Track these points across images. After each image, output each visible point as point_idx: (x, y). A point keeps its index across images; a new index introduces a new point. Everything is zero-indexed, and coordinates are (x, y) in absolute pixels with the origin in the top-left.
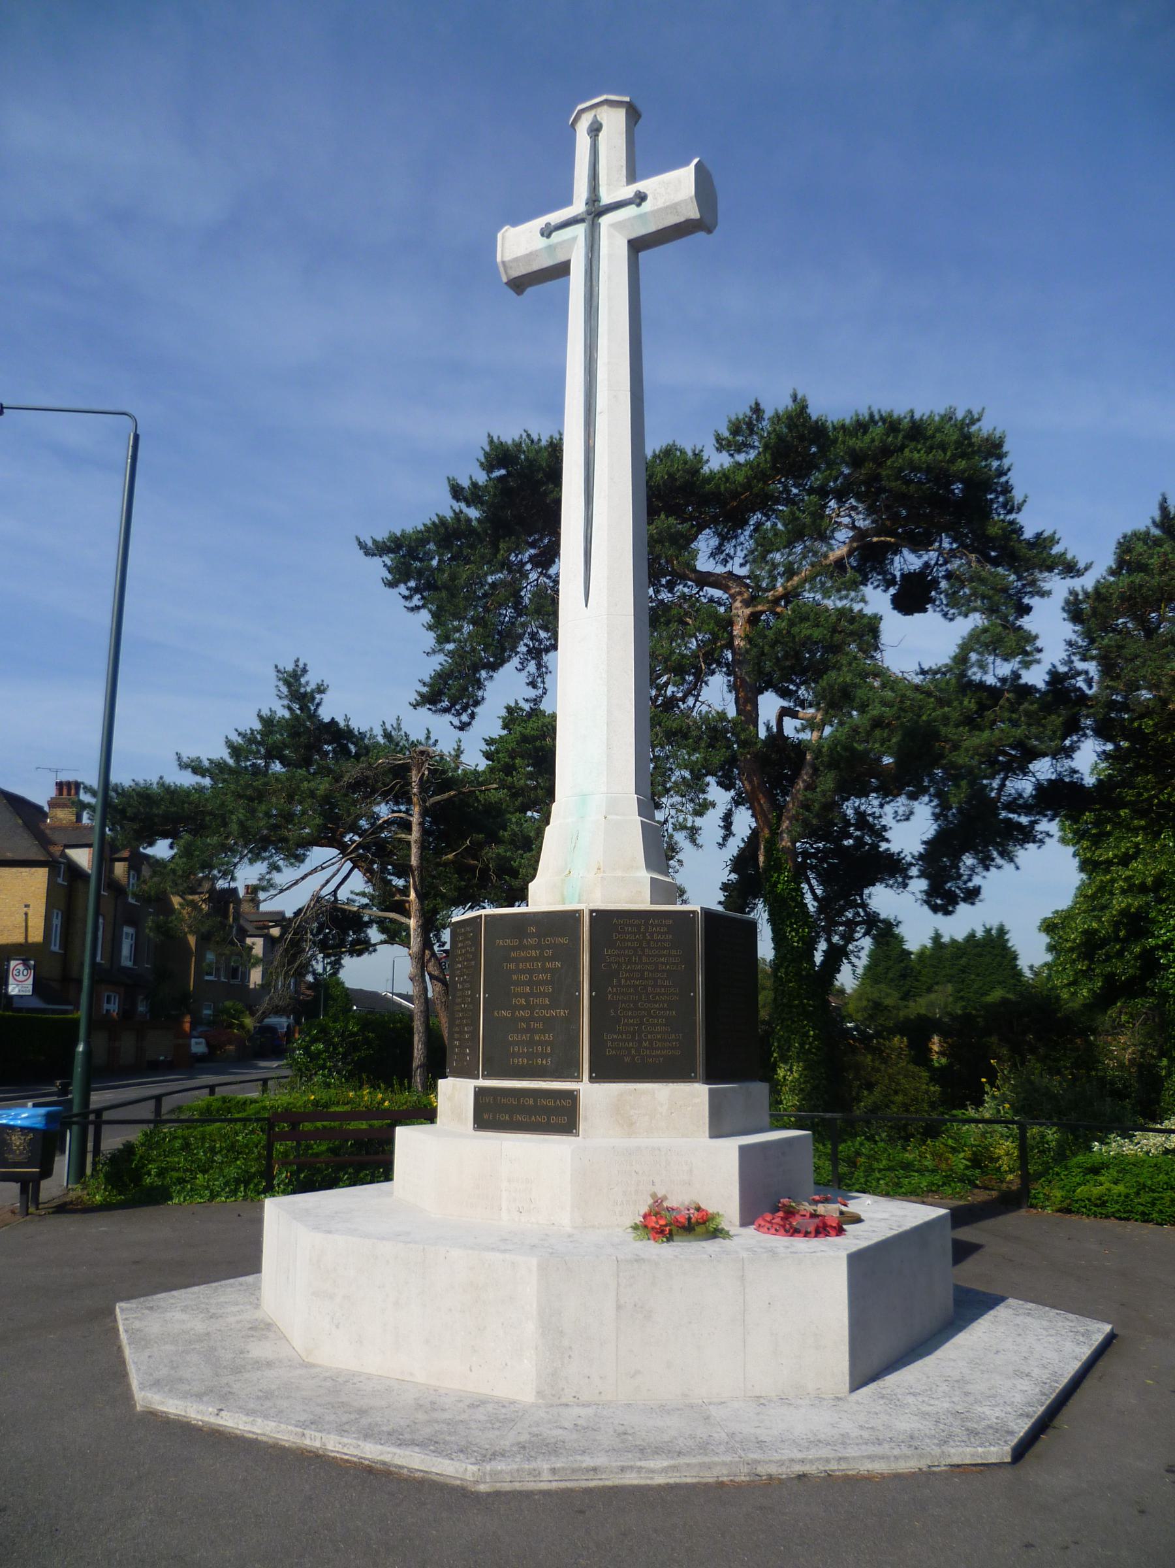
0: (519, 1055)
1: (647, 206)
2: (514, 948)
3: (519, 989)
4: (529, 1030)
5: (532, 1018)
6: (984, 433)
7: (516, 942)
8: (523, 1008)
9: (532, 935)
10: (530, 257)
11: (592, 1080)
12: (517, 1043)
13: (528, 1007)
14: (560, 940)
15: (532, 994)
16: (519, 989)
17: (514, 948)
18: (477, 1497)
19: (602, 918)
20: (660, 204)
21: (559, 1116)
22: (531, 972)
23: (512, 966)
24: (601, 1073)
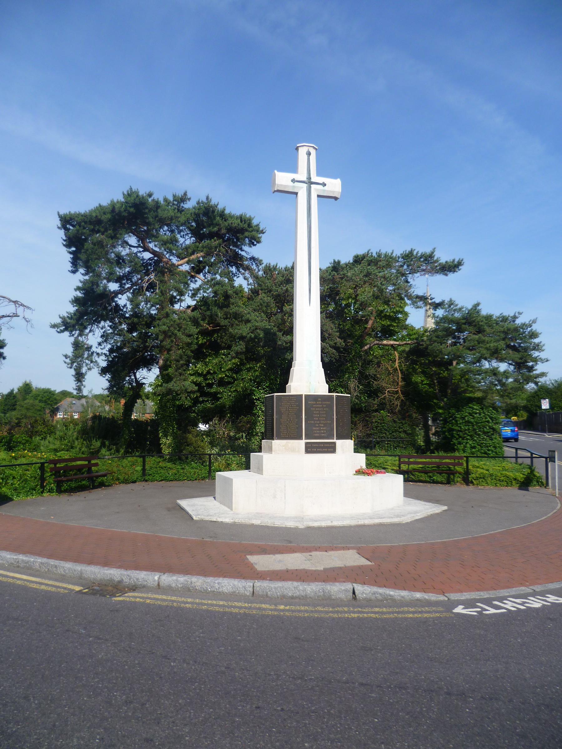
0: (316, 433)
1: (326, 188)
2: (314, 404)
3: (316, 415)
4: (319, 426)
5: (320, 423)
6: (213, 204)
7: (315, 403)
8: (317, 421)
9: (319, 401)
10: (285, 186)
11: (336, 439)
12: (316, 430)
13: (318, 420)
14: (328, 403)
15: (320, 417)
16: (316, 415)
17: (314, 404)
18: (384, 525)
19: (306, 396)
20: (330, 189)
21: (332, 449)
22: (319, 411)
23: (314, 409)
24: (338, 438)
